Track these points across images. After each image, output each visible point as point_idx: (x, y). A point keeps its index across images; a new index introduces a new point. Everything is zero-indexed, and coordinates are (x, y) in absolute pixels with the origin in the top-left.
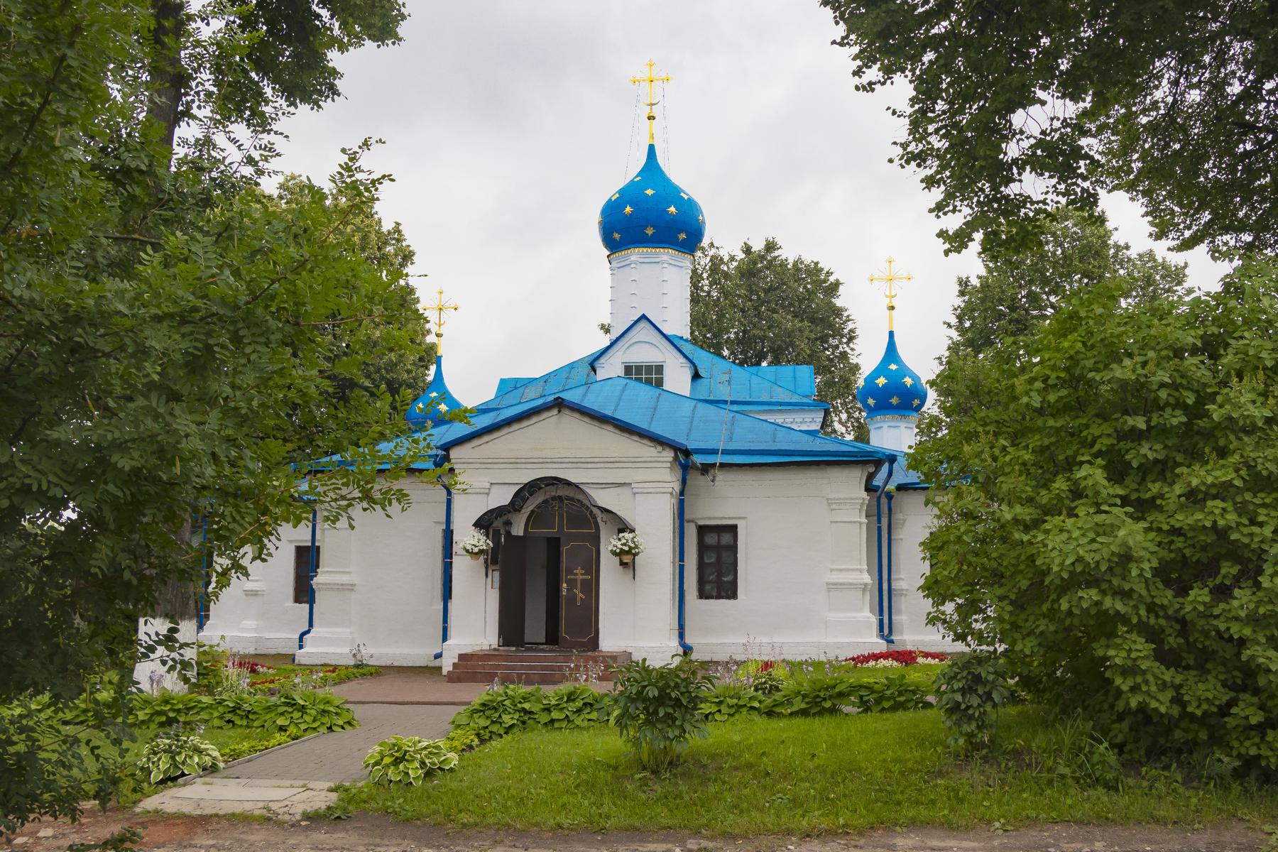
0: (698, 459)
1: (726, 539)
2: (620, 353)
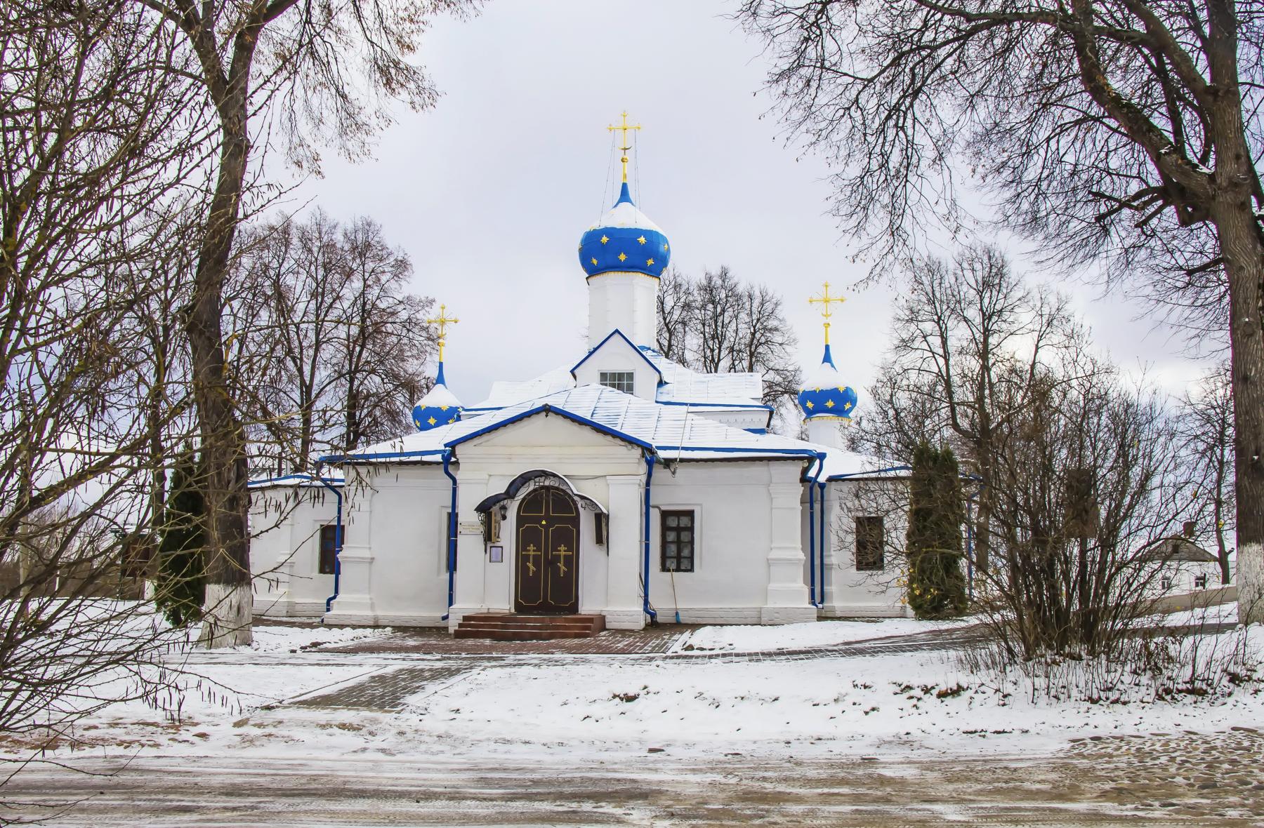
0: (662, 454)
1: (684, 521)
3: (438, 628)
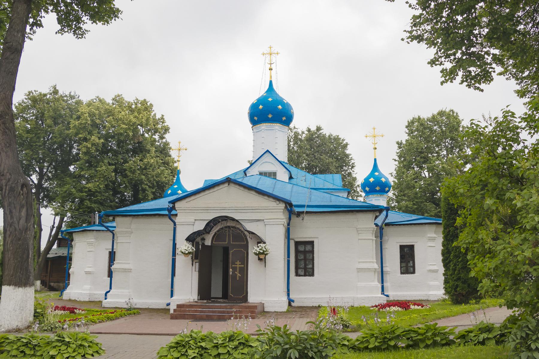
0: (297, 210)
1: (308, 248)
2: (257, 167)
3: (165, 309)
